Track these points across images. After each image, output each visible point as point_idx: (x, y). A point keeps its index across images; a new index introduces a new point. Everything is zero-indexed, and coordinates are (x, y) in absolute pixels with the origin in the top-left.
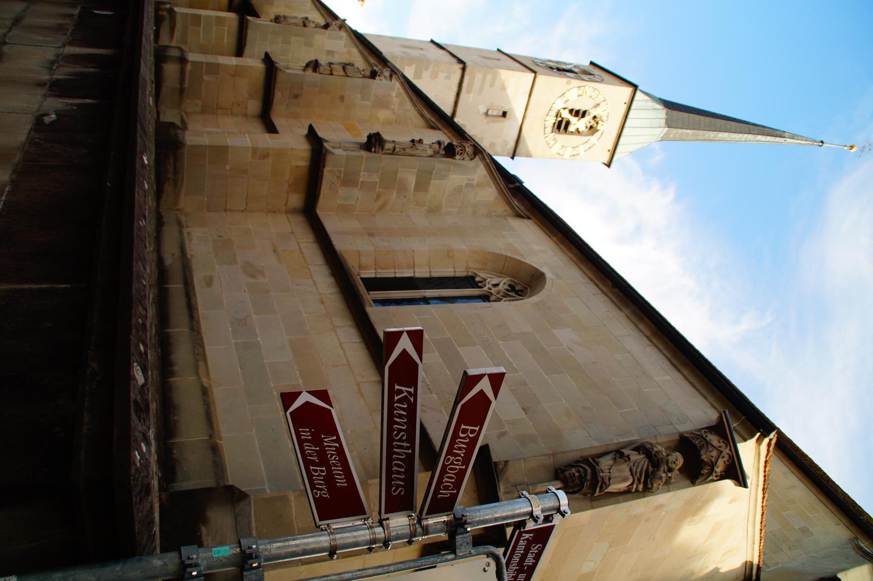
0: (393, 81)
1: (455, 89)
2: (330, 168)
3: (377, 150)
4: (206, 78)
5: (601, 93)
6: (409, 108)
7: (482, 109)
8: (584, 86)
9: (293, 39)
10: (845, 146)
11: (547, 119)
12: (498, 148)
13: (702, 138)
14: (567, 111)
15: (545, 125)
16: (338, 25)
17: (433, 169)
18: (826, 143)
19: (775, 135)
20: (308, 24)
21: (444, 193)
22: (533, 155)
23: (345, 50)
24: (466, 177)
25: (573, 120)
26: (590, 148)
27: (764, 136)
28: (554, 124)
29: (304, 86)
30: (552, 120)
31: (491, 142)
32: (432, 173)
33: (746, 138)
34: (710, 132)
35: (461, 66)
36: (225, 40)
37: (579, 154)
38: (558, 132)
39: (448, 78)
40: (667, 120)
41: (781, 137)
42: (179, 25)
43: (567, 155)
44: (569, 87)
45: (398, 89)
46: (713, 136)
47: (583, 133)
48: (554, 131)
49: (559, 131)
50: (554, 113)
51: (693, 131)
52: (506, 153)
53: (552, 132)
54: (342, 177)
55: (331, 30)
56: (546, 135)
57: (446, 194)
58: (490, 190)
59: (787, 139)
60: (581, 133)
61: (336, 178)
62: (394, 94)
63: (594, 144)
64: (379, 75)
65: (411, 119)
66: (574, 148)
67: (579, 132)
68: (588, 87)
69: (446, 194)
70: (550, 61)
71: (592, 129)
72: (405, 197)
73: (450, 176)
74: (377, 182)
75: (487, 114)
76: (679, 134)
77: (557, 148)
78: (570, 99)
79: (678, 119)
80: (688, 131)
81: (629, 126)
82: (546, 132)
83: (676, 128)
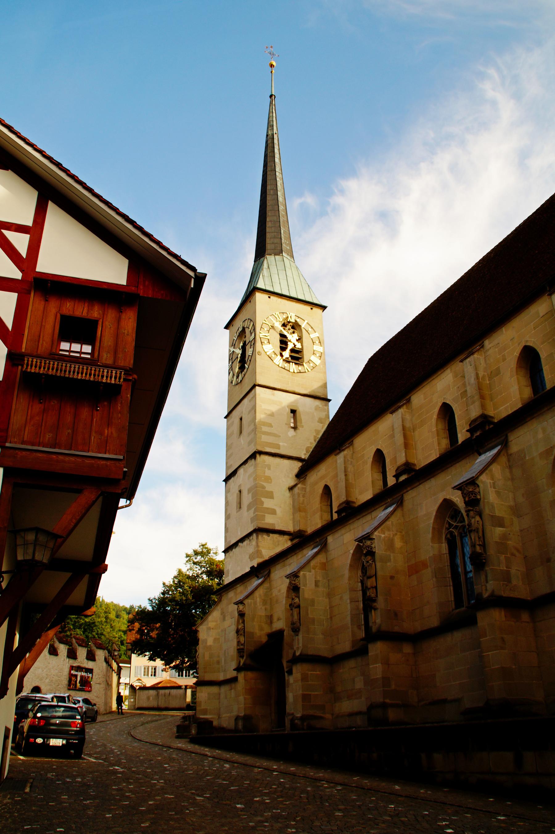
0: (374, 538)
1: (278, 460)
2: (503, 592)
3: (484, 558)
4: (393, 687)
5: (264, 322)
6: (390, 522)
7: (292, 432)
8: (260, 338)
9: (310, 616)
10: (271, 72)
11: (293, 371)
12: (323, 415)
13: (286, 217)
14: (284, 353)
15: (297, 373)
16: (294, 579)
17: (490, 515)
18: (271, 93)
19: (272, 144)
20: (297, 604)
21: (502, 504)
22: (324, 382)
23: (313, 571)
24: (490, 489)
25: (290, 346)
26: (312, 328)
27: (275, 156)
28: (296, 364)
29: (388, 609)
30: (293, 367)
31: (318, 422)
32: (492, 515)
33: (279, 173)
34: (280, 210)
35: (258, 456)
36: (318, 673)
37: (318, 337)
38: (302, 359)
39: (269, 467)
40: (275, 255)
41: (273, 138)
42: (311, 712)
43: (320, 349)
44: (263, 353)
45: (379, 532)
46: (282, 207)
47: (299, 335)
48: (302, 364)
49: (301, 358)
50: (286, 365)
51: (281, 227)
52: (326, 407)
53: (303, 365)
54: (506, 583)
55: (300, 584)
56: (307, 371)
57: (503, 503)
58: (493, 469)
59: (274, 133)
60: (300, 336)
61: (508, 587)
62: (383, 536)
63: (295, 316)
64: (371, 549)
65: (398, 520)
66: (313, 343)
67: (299, 339)
68: (261, 334)
69: (503, 503)
70: (231, 368)
71: (295, 327)
72: (509, 534)
73: (491, 501)
74: (505, 556)
75: (295, 428)
76: (286, 241)
77: (315, 359)
78: (273, 350)
79: (273, 243)
80: (282, 232)
81: (296, 295)
82: (304, 371)
83: (282, 244)
